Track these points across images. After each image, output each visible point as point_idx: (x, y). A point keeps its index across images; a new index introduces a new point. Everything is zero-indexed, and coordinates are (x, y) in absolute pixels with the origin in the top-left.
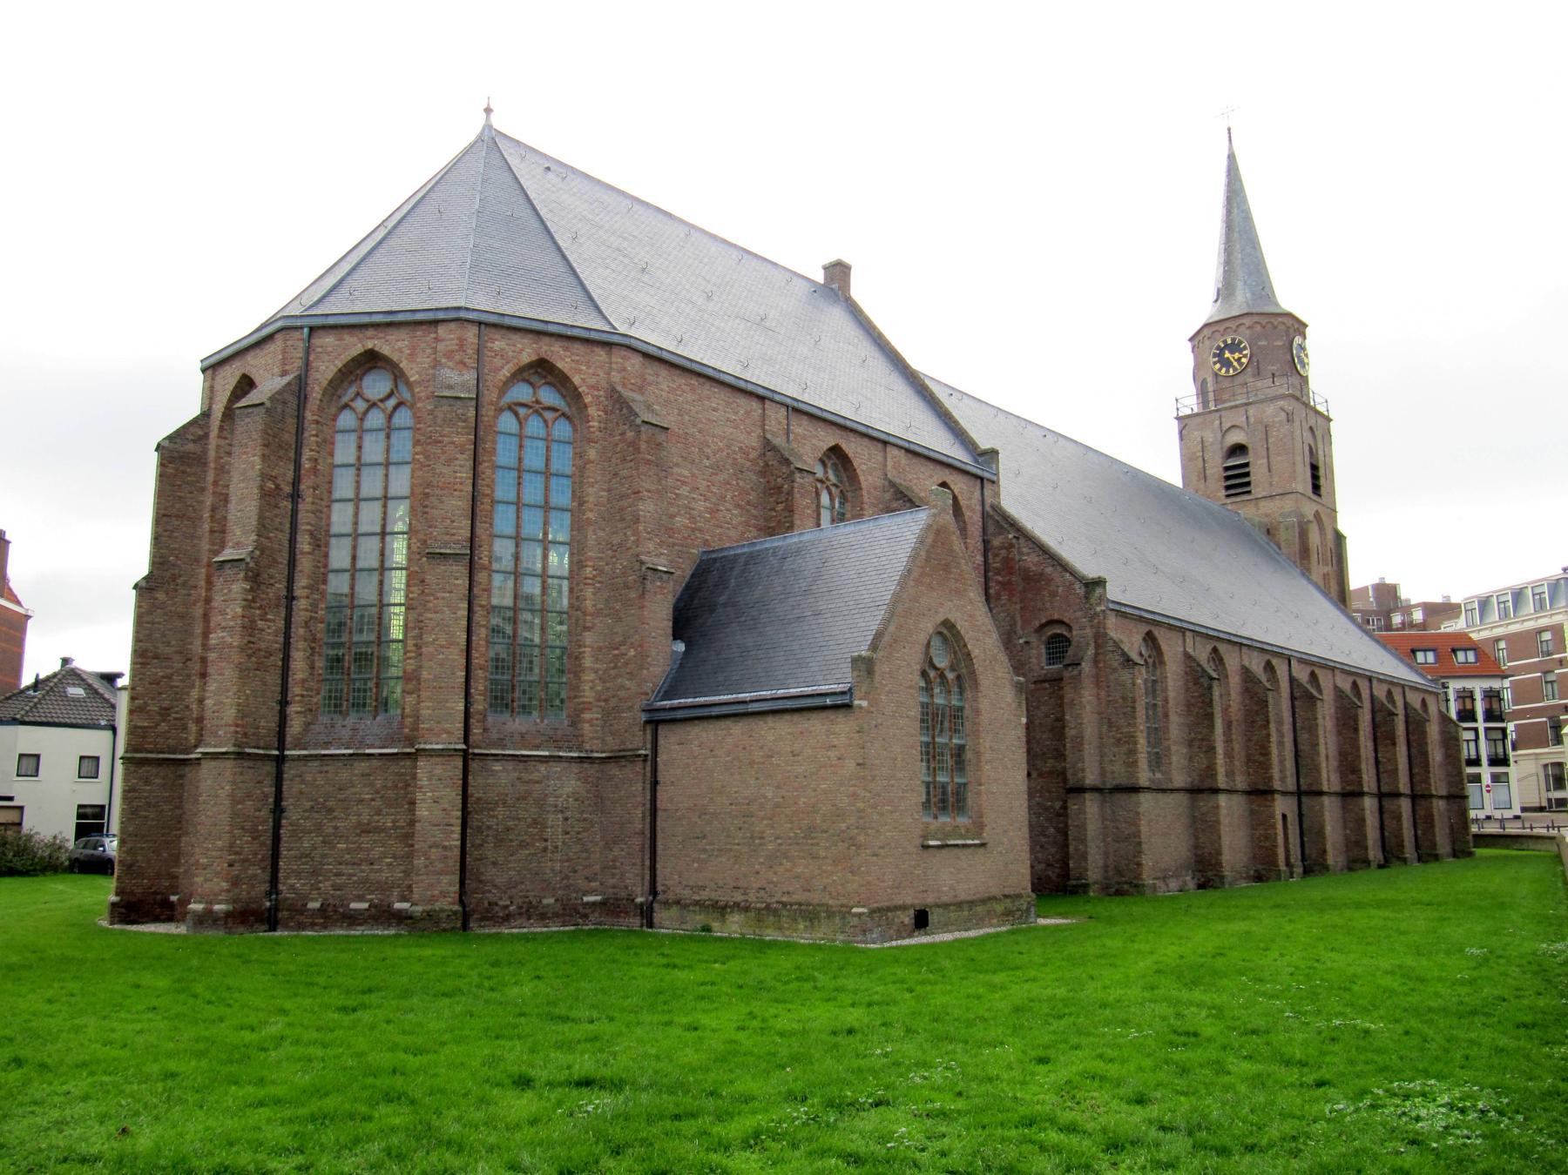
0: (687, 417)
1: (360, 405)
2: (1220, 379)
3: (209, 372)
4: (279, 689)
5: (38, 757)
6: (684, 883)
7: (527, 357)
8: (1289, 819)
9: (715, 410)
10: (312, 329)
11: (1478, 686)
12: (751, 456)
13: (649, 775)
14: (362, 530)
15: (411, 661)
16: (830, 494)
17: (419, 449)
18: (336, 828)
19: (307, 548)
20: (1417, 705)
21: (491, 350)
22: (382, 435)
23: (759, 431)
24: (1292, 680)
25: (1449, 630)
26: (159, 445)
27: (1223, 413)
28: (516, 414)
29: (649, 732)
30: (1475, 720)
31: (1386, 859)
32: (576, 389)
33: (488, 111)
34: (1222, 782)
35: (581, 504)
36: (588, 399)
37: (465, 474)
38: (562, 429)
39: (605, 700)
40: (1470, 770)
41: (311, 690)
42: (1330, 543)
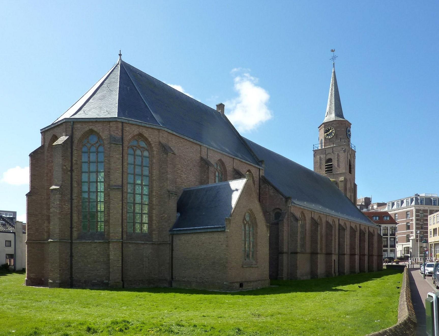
0: (180, 151)
1: (89, 145)
2: (326, 139)
3: (43, 133)
7: (136, 132)
8: (336, 261)
9: (188, 149)
10: (73, 122)
11: (389, 226)
13: (171, 248)
14: (91, 180)
15: (106, 217)
16: (218, 172)
17: (106, 158)
18: (87, 261)
19: (76, 186)
20: (372, 231)
22: (95, 154)
23: (200, 155)
24: (339, 225)
25: (383, 211)
26: (30, 154)
27: (326, 149)
28: (133, 149)
30: (388, 236)
32: (150, 142)
33: (120, 55)
36: (153, 145)
37: (120, 166)
38: (146, 154)
40: (384, 249)
42: (353, 187)
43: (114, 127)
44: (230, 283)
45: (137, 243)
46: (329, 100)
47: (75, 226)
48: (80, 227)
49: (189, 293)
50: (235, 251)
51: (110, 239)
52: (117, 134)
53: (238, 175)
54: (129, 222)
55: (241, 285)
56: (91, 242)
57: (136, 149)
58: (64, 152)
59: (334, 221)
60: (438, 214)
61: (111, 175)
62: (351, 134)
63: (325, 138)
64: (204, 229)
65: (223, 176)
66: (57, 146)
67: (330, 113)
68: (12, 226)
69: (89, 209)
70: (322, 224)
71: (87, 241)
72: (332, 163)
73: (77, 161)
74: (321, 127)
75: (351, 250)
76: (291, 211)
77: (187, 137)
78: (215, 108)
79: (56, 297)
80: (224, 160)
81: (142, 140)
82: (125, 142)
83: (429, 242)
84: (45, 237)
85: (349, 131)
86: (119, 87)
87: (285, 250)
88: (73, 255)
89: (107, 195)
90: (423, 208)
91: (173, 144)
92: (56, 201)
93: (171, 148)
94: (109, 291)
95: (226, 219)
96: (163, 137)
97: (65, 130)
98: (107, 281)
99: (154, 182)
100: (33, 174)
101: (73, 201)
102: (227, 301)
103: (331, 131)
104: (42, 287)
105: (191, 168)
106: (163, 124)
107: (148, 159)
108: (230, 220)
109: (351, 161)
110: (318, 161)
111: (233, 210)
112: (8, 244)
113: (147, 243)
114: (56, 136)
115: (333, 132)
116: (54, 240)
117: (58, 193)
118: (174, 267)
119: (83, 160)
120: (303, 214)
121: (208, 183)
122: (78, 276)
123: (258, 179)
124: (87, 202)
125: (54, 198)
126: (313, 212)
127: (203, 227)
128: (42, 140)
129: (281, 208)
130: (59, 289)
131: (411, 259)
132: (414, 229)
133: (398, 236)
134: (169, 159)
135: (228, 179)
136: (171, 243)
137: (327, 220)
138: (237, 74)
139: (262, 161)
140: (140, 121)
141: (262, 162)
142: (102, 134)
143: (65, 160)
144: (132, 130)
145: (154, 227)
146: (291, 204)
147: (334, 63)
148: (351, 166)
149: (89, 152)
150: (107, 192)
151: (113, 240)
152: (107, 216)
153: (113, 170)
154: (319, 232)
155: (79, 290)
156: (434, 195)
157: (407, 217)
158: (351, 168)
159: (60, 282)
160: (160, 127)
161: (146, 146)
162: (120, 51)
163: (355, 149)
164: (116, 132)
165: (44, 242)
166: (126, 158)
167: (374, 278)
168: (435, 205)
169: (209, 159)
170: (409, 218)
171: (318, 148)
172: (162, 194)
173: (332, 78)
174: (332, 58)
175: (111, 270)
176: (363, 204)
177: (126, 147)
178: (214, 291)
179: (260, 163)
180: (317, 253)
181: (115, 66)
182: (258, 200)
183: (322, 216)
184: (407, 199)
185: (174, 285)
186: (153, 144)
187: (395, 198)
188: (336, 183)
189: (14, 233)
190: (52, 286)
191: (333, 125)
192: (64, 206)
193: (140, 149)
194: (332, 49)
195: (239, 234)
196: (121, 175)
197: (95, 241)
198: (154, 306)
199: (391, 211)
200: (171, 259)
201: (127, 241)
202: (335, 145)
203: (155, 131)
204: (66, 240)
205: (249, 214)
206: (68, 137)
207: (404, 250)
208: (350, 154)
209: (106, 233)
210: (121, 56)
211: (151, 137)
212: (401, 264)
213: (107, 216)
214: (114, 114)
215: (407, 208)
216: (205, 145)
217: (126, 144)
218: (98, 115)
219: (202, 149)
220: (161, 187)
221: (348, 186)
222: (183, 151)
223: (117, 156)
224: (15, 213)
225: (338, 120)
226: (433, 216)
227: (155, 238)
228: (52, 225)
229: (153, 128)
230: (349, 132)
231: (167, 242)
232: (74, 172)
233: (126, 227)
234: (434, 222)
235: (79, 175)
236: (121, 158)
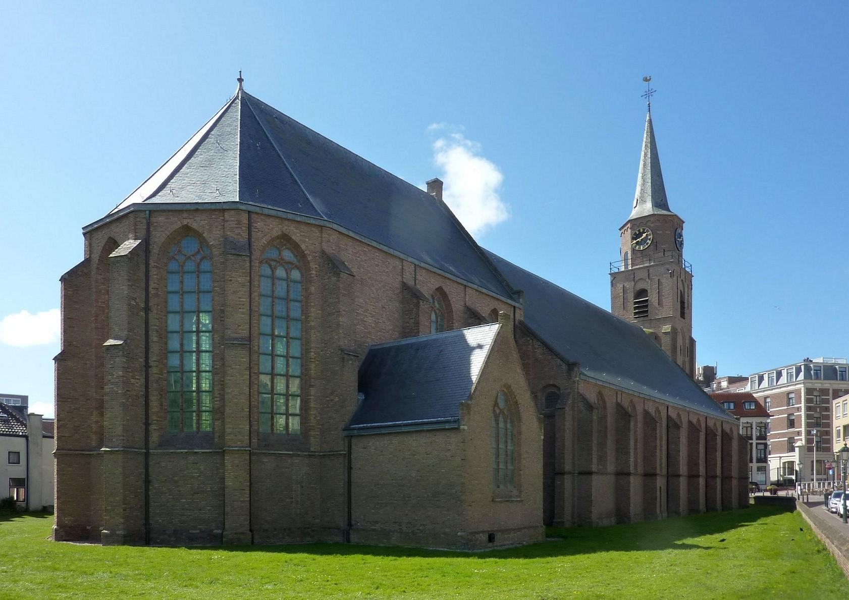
0: (362, 270)
1: (181, 258)
3: (87, 235)
4: (144, 416)
5: (19, 452)
9: (377, 265)
10: (150, 211)
11: (755, 421)
12: (395, 292)
16: (436, 314)
19: (155, 339)
20: (728, 431)
22: (194, 276)
23: (400, 278)
24: (668, 417)
25: (740, 391)
27: (636, 272)
28: (270, 266)
29: (346, 442)
31: (707, 510)
33: (240, 80)
34: (632, 470)
36: (310, 258)
37: (245, 300)
38: (296, 275)
39: (322, 425)
43: (232, 221)
44: (471, 533)
46: (640, 175)
47: (155, 420)
48: (164, 423)
49: (393, 556)
52: (238, 235)
53: (476, 319)
54: (262, 413)
55: (491, 538)
56: (186, 452)
57: (276, 266)
58: (131, 272)
59: (658, 410)
60: (846, 400)
61: (227, 318)
62: (683, 241)
63: (633, 250)
64: (439, 423)
65: (446, 320)
66: (116, 259)
67: (642, 200)
68: (22, 424)
69: (182, 386)
71: (179, 451)
74: (625, 228)
76: (580, 391)
78: (424, 188)
79: (121, 565)
80: (446, 289)
81: (287, 248)
82: (255, 251)
83: (834, 451)
84: (94, 444)
85: (681, 236)
86: (241, 143)
87: (568, 467)
88: (150, 478)
89: (218, 357)
90: (820, 385)
92: (115, 371)
93: (346, 263)
94: (227, 551)
95: (462, 404)
96: (329, 241)
97: (133, 228)
98: (219, 531)
99: (313, 331)
102: (476, 571)
103: (644, 235)
104: (88, 544)
106: (329, 216)
107: (299, 286)
108: (468, 407)
111: (474, 387)
112: (14, 458)
113: (299, 453)
114: (115, 240)
115: (649, 237)
116: (112, 449)
117: (121, 352)
118: (353, 501)
119: (170, 289)
121: (417, 333)
124: (179, 372)
125: (111, 364)
126: (619, 393)
127: (413, 421)
128: (87, 248)
130: (124, 547)
131: (800, 485)
132: (803, 426)
133: (771, 441)
134: (341, 286)
135: (454, 327)
136: (347, 455)
137: (646, 408)
138: (438, 135)
139: (520, 292)
140: (284, 210)
141: (519, 293)
142: (208, 234)
143: (133, 287)
144: (268, 227)
145: (313, 422)
146: (578, 376)
147: (649, 104)
148: (684, 303)
149: (182, 272)
150: (218, 352)
151: (231, 449)
152: (219, 401)
154: (632, 432)
155: (165, 549)
156: (840, 361)
157: (788, 404)
158: (684, 308)
159: (126, 533)
161: (295, 260)
162: (240, 72)
165: (92, 453)
166: (256, 283)
167: (744, 522)
168: (843, 379)
169: (418, 287)
170: (792, 405)
171: (618, 269)
172: (328, 355)
173: (645, 132)
174: (652, 94)
175: (228, 509)
177: (256, 261)
178: (437, 549)
179: (515, 296)
180: (629, 474)
181: (231, 101)
182: (521, 368)
183: (636, 400)
184: (788, 367)
185: (354, 538)
186: (309, 255)
187: (765, 366)
188: (656, 337)
189: (26, 437)
190: (110, 540)
191: (649, 224)
192: (132, 380)
193: (283, 266)
195: (487, 435)
196: (248, 318)
197: (195, 451)
198: (329, 583)
199: (757, 392)
200: (346, 487)
201: (259, 450)
202: (653, 263)
203: (313, 229)
205: (505, 394)
206: (140, 241)
207: (784, 468)
208: (682, 280)
209: (217, 435)
212: (782, 493)
213: (218, 399)
214: (234, 196)
215: (788, 386)
216: (410, 259)
217: (256, 254)
218: (199, 197)
219: (404, 268)
220: (326, 342)
221: (680, 342)
223: (238, 279)
224: (25, 399)
225: (658, 215)
226: (843, 401)
227: (314, 443)
228: (107, 418)
229: (309, 224)
230: (680, 238)
231: (339, 453)
233: (256, 423)
234: (846, 413)
236: (248, 284)
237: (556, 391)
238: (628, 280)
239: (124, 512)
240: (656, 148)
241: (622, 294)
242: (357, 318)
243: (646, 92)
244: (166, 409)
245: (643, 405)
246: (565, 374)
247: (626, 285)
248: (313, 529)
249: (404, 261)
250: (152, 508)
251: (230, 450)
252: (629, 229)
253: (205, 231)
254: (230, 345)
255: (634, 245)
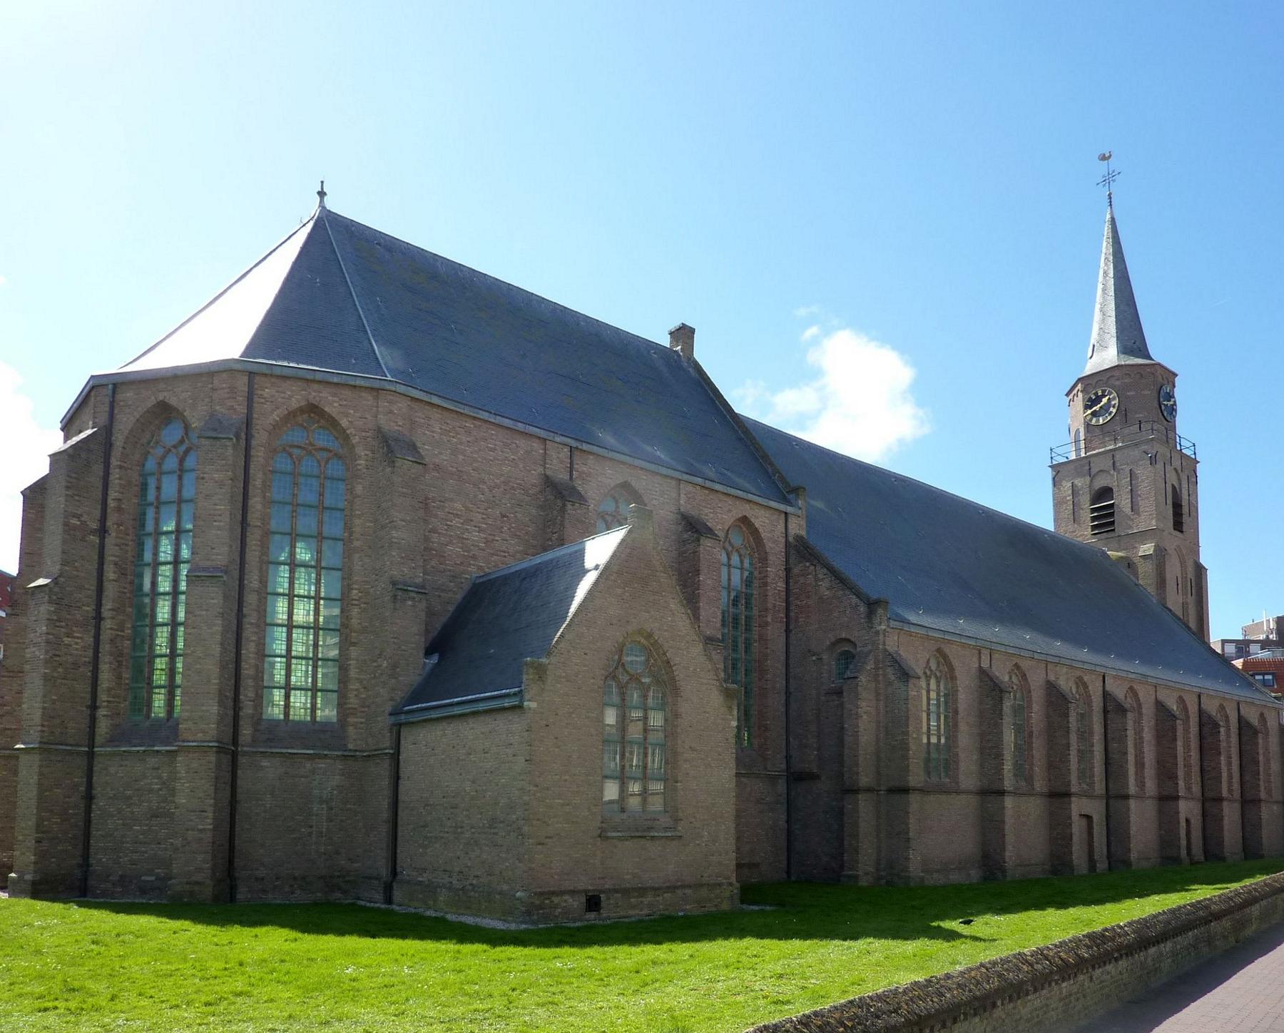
0: (461, 457)
2: (1090, 428)
6: (413, 865)
10: (115, 385)
18: (132, 813)
20: (1255, 721)
21: (261, 396)
22: (175, 477)
24: (1106, 695)
27: (1092, 460)
28: (290, 455)
32: (344, 431)
33: (322, 194)
35: (351, 534)
36: (355, 440)
41: (118, 697)
43: (223, 388)
45: (290, 753)
47: (104, 702)
50: (567, 777)
51: (179, 741)
56: (144, 751)
63: (1088, 426)
70: (1030, 692)
72: (1112, 502)
73: (119, 500)
75: (1160, 784)
76: (887, 647)
77: (487, 414)
78: (665, 341)
81: (321, 427)
85: (1170, 396)
87: (865, 780)
91: (435, 435)
100: (28, 551)
101: (102, 622)
103: (1105, 400)
105: (503, 513)
109: (1181, 491)
110: (1066, 497)
113: (325, 753)
115: (1113, 403)
120: (945, 657)
122: (104, 860)
123: (782, 545)
129: (853, 640)
137: (1052, 678)
141: (796, 490)
143: (77, 498)
147: (1110, 195)
151: (186, 744)
153: (204, 521)
159: (38, 878)
160: (378, 381)
162: (322, 182)
163: (1195, 454)
164: (229, 403)
176: (1273, 637)
177: (260, 448)
179: (791, 497)
180: (1002, 793)
182: (681, 601)
183: (1025, 664)
186: (355, 435)
188: (1130, 565)
191: (1112, 381)
194: (1104, 152)
197: (156, 748)
201: (254, 747)
202: (1120, 445)
203: (363, 394)
204: (71, 745)
210: (325, 198)
211: (350, 414)
216: (558, 439)
217: (260, 438)
219: (547, 452)
221: (1173, 570)
222: (472, 458)
223: (215, 476)
225: (1126, 365)
227: (354, 738)
229: (355, 386)
230: (1170, 401)
232: (110, 535)
235: (127, 545)
237: (851, 650)
238: (1079, 474)
239: (37, 845)
240: (1124, 261)
241: (1071, 497)
242: (449, 533)
243: (1104, 176)
244: (127, 684)
245: (1044, 672)
246: (862, 620)
247: (1076, 482)
248: (347, 879)
249: (547, 442)
250: (94, 838)
251: (185, 746)
252: (1079, 393)
253: (187, 408)
254: (194, 578)
255: (1088, 418)
